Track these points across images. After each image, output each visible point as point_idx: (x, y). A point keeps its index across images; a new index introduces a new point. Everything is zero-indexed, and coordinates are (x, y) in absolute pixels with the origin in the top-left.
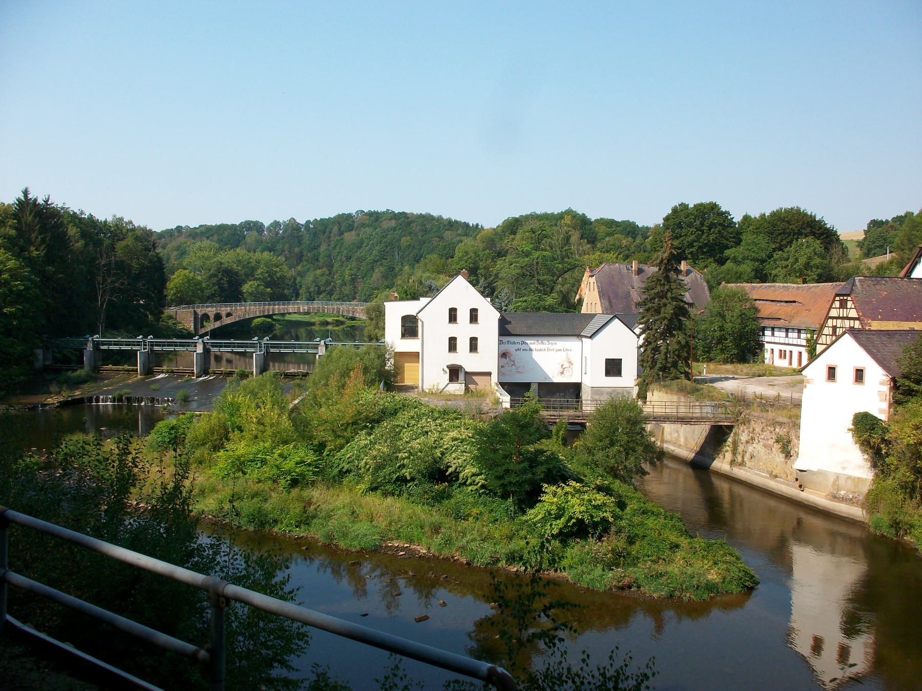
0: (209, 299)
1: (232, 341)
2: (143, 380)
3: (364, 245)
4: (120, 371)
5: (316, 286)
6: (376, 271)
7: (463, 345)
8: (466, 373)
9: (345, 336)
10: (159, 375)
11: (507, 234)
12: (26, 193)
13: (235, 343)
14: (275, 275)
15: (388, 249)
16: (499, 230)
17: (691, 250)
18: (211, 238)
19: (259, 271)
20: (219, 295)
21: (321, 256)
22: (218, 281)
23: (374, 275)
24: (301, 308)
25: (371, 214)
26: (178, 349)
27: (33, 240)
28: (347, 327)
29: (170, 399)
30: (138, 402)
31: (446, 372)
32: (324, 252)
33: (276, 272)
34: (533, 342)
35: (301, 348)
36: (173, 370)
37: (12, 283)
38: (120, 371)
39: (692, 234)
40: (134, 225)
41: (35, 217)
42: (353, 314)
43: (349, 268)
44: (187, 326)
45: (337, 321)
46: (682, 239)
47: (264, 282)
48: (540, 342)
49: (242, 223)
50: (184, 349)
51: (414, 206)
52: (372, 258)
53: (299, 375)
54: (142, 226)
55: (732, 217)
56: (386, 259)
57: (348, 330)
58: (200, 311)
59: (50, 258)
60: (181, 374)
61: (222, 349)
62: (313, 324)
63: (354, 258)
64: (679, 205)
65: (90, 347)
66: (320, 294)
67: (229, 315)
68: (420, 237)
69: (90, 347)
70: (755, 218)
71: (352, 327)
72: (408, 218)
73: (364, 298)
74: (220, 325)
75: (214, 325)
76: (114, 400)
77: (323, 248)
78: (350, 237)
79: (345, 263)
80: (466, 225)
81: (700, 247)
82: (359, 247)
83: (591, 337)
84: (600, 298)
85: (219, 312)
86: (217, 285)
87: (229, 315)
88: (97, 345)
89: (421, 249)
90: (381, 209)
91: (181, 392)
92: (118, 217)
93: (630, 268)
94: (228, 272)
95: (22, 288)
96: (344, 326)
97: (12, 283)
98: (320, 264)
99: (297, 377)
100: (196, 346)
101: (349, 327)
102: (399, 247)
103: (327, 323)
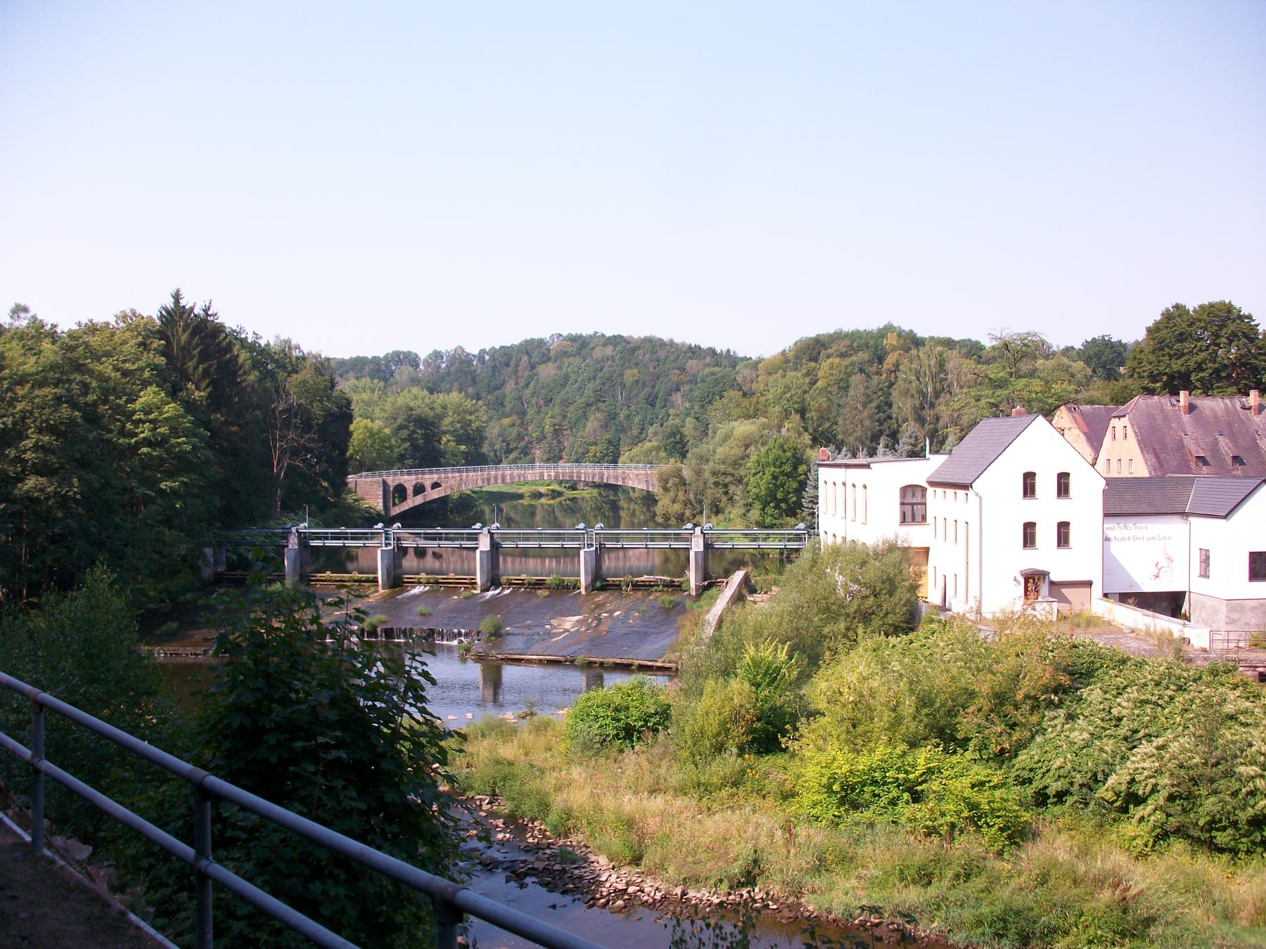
0: (400, 461)
1: (343, 529)
2: (392, 596)
3: (569, 383)
5: (504, 441)
6: (592, 418)
7: (1046, 535)
8: (1052, 583)
10: (414, 587)
11: (804, 360)
12: (177, 297)
13: (347, 533)
14: (470, 425)
15: (606, 387)
16: (790, 355)
17: (1201, 374)
18: (345, 376)
19: (447, 421)
20: (412, 457)
21: (507, 399)
22: (409, 435)
23: (589, 425)
24: (546, 475)
25: (573, 339)
26: (349, 543)
27: (190, 371)
28: (565, 500)
29: (463, 631)
30: (405, 636)
31: (1019, 583)
32: (511, 393)
33: (470, 421)
34: (1111, 526)
35: (528, 539)
36: (437, 579)
37: (173, 441)
39: (1201, 350)
40: (302, 351)
41: (193, 334)
42: (624, 482)
43: (549, 415)
44: (373, 504)
45: (553, 491)
46: (1185, 358)
47: (453, 436)
48: (1122, 525)
49: (388, 354)
50: (360, 543)
51: (635, 329)
52: (583, 400)
53: (658, 586)
54: (314, 352)
55: (1255, 323)
56: (604, 402)
58: (393, 479)
59: (217, 400)
60: (452, 587)
61: (444, 543)
62: (521, 496)
63: (558, 400)
64: (1173, 307)
65: (293, 542)
66: (510, 453)
67: (436, 485)
68: (651, 369)
69: (293, 542)
71: (573, 500)
72: (629, 343)
73: (574, 457)
74: (422, 502)
75: (413, 501)
77: (510, 387)
78: (547, 372)
79: (544, 408)
80: (712, 352)
81: (1217, 371)
82: (564, 386)
83: (1225, 517)
84: (1142, 451)
85: (420, 481)
86: (408, 441)
87: (436, 485)
88: (303, 539)
89: (654, 386)
90: (586, 331)
91: (488, 620)
92: (282, 338)
93: (1175, 403)
94: (421, 422)
95: (189, 448)
96: (563, 498)
97: (173, 441)
98: (507, 409)
99: (655, 588)
100: (476, 539)
102: (623, 385)
103: (540, 495)
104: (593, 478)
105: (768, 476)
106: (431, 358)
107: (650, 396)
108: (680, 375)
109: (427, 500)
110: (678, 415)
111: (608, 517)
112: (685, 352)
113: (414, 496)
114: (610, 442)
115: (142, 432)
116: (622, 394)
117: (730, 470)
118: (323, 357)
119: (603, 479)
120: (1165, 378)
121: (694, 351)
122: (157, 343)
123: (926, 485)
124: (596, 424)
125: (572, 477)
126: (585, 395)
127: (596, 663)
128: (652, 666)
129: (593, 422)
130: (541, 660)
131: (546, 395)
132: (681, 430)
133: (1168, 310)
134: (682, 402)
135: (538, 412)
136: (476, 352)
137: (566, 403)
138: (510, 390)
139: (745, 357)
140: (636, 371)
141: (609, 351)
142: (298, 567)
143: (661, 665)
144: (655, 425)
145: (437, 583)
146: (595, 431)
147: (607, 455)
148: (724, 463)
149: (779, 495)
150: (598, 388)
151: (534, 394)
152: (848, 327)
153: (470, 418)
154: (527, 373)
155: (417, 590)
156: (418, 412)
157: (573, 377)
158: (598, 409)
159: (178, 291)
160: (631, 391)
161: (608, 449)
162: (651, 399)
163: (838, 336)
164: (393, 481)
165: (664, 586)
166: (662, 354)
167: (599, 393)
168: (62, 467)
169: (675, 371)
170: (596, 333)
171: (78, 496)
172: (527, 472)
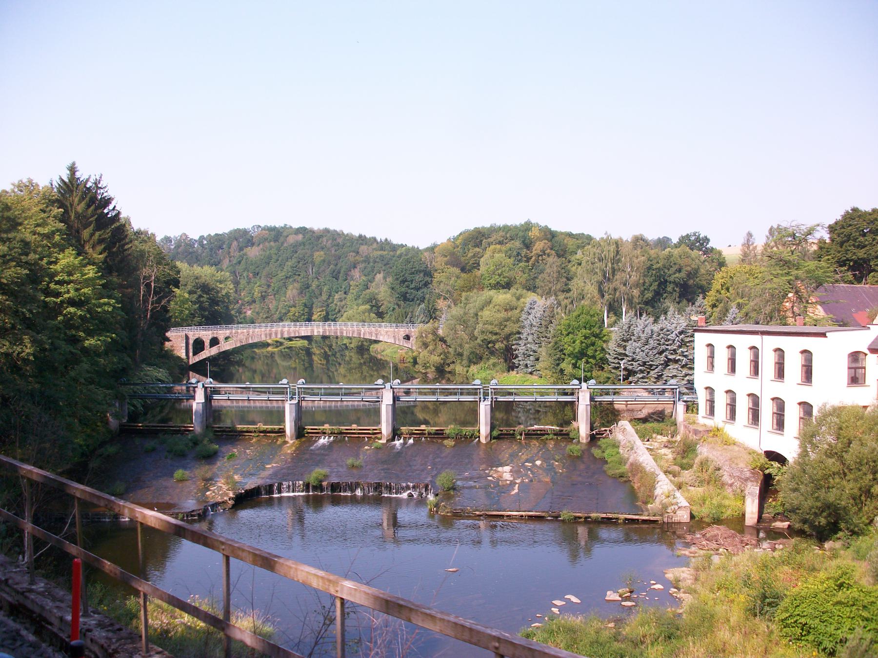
4: (251, 432)
6: (290, 287)
9: (283, 358)
12: (73, 169)
15: (300, 265)
22: (197, 299)
28: (284, 348)
38: (251, 432)
42: (377, 337)
43: (258, 284)
51: (316, 224)
52: (284, 274)
53: (548, 434)
56: (299, 275)
57: (286, 352)
62: (268, 345)
70: (627, 241)
71: (290, 348)
76: (307, 487)
85: (215, 336)
89: (337, 264)
90: (278, 223)
101: (287, 348)
104: (353, 334)
105: (579, 338)
106: (162, 242)
107: (334, 271)
108: (355, 257)
109: (221, 351)
110: (357, 286)
111: (303, 361)
112: (357, 240)
113: (210, 347)
114: (305, 305)
115: (68, 292)
116: (312, 269)
117: (496, 330)
118: (149, 233)
119: (360, 334)
120: (851, 264)
121: (362, 239)
122: (57, 211)
123: (867, 352)
124: (295, 292)
125: (336, 332)
126: (285, 270)
127: (580, 518)
128: (638, 520)
129: (292, 291)
130: (522, 516)
131: (254, 270)
132: (376, 297)
133: (847, 212)
134: (360, 277)
135: (249, 283)
136: (197, 238)
137: (270, 276)
138: (226, 266)
139: (402, 245)
140: (322, 253)
141: (300, 237)
142: (205, 419)
143: (647, 518)
144: (340, 293)
145: (341, 433)
146: (294, 297)
147: (303, 314)
148: (491, 324)
149: (590, 352)
150: (294, 265)
151: (245, 269)
152: (500, 222)
153: (220, 286)
154: (237, 254)
155: (323, 441)
156: (202, 280)
157: (274, 257)
158: (295, 280)
159: (74, 164)
160: (319, 268)
161: (303, 310)
162: (335, 273)
163: (493, 230)
164: (194, 335)
165: (555, 434)
166: (340, 241)
167: (295, 269)
168: (13, 327)
169: (351, 253)
170: (286, 225)
171: (31, 358)
172: (301, 329)
